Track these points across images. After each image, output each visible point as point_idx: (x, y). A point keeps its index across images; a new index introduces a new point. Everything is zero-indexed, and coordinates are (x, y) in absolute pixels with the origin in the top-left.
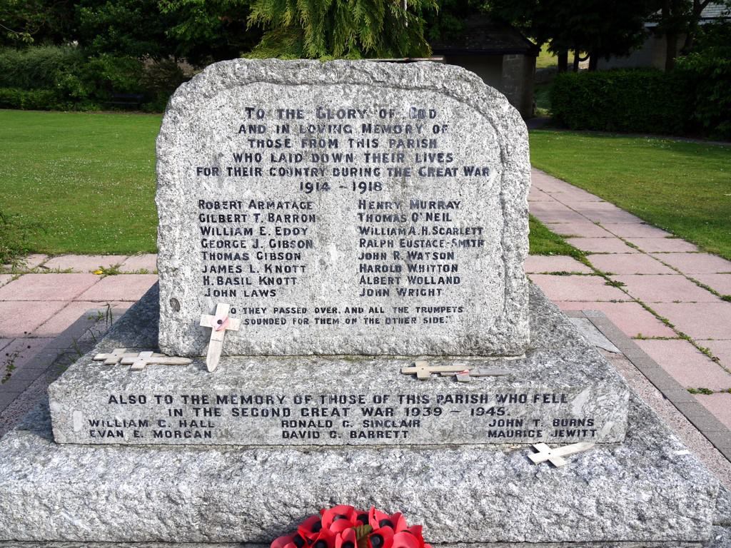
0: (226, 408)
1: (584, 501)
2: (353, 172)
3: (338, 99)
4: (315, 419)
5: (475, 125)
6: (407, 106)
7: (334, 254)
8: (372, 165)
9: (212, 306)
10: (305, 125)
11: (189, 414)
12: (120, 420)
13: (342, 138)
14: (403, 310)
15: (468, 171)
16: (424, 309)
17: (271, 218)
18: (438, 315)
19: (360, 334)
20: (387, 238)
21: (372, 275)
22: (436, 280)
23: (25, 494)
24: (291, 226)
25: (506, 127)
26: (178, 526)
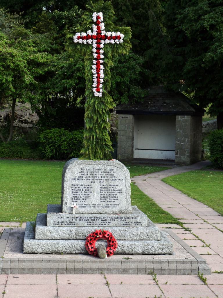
0: (78, 219)
1: (138, 232)
2: (99, 180)
3: (97, 167)
4: (93, 221)
5: (120, 172)
6: (109, 168)
7: (95, 194)
8: (102, 178)
9: (73, 204)
10: (91, 171)
11: (71, 221)
12: (59, 222)
13: (97, 174)
14: (108, 205)
15: (119, 180)
16: (112, 205)
17: (84, 188)
18: (114, 206)
19: (100, 210)
20: (105, 191)
21: (102, 198)
22: (114, 199)
23: (47, 230)
24: (88, 189)
25: (126, 172)
26: (72, 236)
